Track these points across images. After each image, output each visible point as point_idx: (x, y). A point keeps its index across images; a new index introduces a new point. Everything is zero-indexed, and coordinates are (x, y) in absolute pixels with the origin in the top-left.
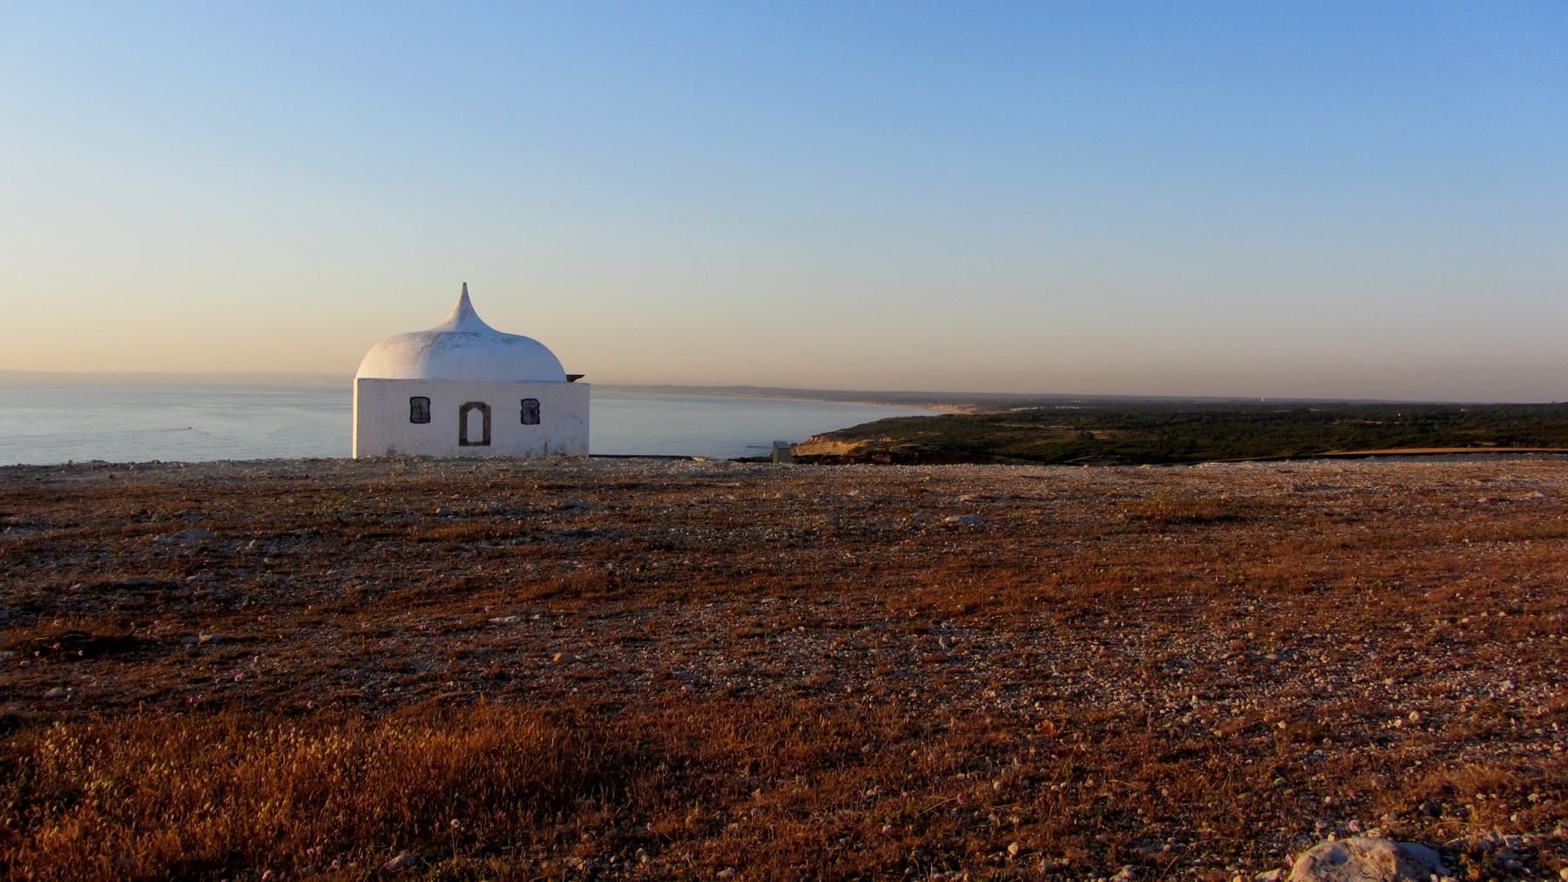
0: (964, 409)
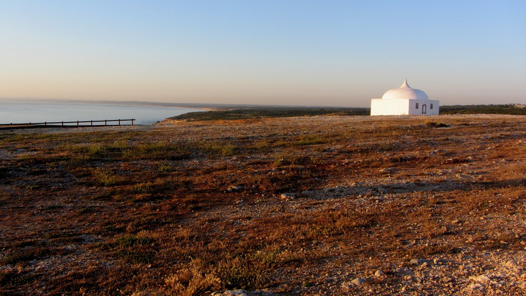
0: (213, 109)
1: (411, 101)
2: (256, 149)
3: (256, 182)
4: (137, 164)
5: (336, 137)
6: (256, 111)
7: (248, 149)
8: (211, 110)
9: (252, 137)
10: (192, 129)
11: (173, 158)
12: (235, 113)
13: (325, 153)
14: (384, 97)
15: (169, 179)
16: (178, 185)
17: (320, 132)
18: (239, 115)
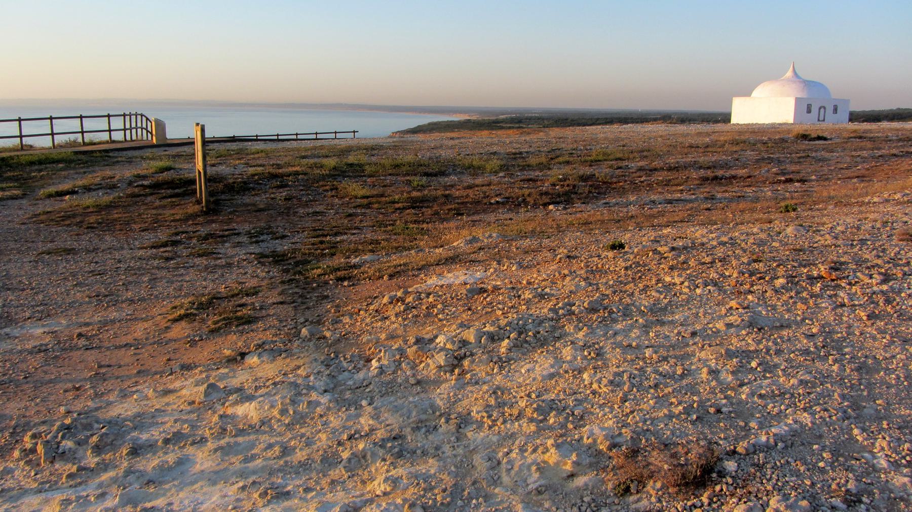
1: (798, 101)
2: (529, 166)
3: (523, 195)
4: (385, 180)
5: (644, 153)
6: (547, 119)
7: (519, 166)
8: (469, 118)
9: (527, 152)
10: (446, 142)
11: (427, 174)
12: (511, 123)
13: (619, 170)
14: (755, 93)
15: (426, 192)
16: (437, 198)
17: (624, 146)
18: (517, 125)
